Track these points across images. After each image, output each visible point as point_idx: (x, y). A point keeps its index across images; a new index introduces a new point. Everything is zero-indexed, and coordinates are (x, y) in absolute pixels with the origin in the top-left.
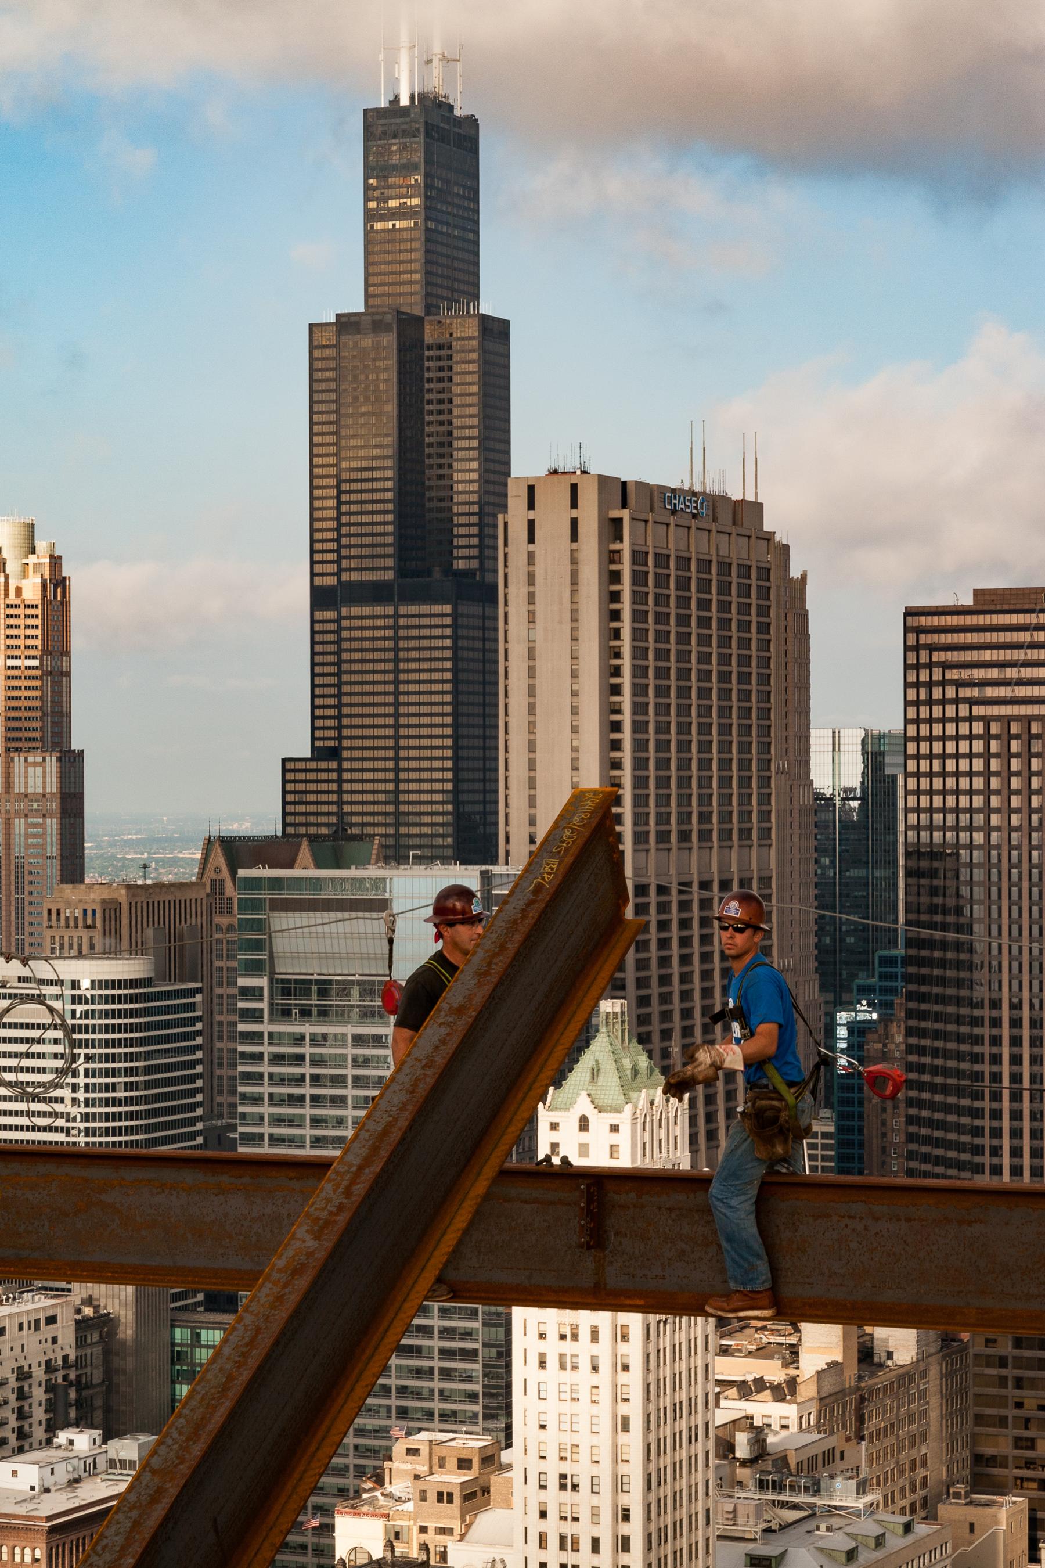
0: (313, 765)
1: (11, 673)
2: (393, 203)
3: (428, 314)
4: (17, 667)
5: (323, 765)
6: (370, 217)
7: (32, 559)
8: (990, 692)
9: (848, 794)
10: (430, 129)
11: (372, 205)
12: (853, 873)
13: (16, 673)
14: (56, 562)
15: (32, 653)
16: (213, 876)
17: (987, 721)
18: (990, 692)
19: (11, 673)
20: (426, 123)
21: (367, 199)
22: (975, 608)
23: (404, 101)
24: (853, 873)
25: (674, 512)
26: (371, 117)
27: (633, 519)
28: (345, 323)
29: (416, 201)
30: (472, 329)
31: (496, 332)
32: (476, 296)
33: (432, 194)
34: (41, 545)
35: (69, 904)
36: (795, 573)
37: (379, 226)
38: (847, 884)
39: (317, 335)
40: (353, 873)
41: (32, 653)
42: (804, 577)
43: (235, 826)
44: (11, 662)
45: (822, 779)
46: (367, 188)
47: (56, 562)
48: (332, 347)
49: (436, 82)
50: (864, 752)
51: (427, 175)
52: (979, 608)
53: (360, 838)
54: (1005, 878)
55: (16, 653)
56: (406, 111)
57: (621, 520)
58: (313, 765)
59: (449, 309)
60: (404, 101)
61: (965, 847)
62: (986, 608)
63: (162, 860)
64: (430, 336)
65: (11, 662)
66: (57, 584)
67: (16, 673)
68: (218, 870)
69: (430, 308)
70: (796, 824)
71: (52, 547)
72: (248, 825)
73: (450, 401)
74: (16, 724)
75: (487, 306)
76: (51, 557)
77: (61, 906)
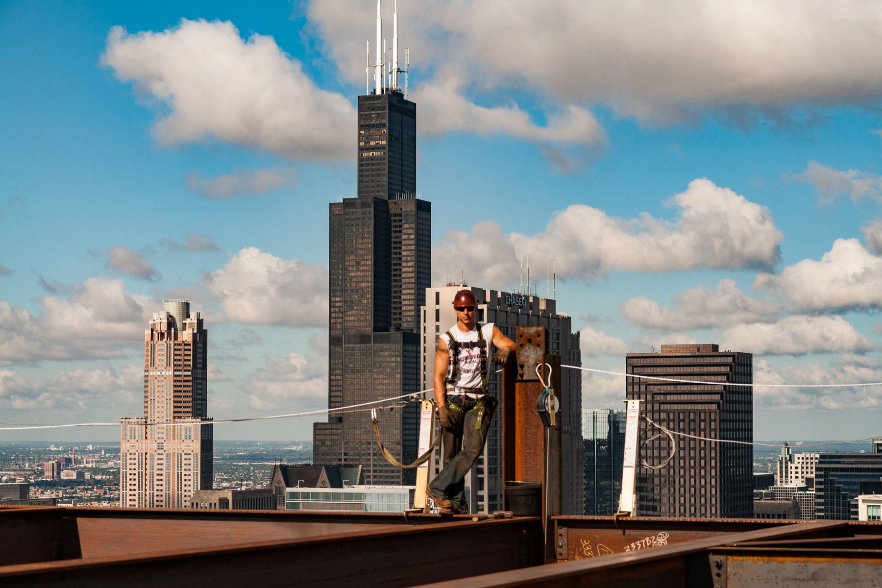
0: (329, 426)
1: (176, 378)
2: (372, 143)
3: (390, 198)
4: (180, 376)
5: (334, 426)
6: (361, 149)
7: (188, 321)
8: (670, 398)
9: (601, 442)
10: (391, 107)
11: (362, 144)
12: (603, 483)
13: (179, 378)
14: (200, 323)
15: (188, 368)
16: (277, 485)
17: (668, 412)
18: (670, 398)
19: (176, 378)
20: (389, 103)
21: (359, 141)
22: (661, 355)
23: (378, 92)
24: (603, 483)
25: (510, 306)
26: (360, 98)
27: (488, 309)
28: (348, 203)
29: (384, 142)
30: (412, 207)
31: (424, 207)
32: (414, 190)
33: (392, 139)
34: (193, 314)
35: (202, 501)
36: (574, 331)
37: (365, 154)
38: (601, 489)
39: (334, 209)
40: (346, 489)
41: (188, 368)
42: (578, 333)
43: (295, 448)
44: (176, 373)
45: (587, 434)
46: (359, 134)
47: (200, 323)
48: (341, 216)
49: (393, 85)
50: (609, 422)
51: (389, 130)
52: (664, 355)
53: (352, 466)
54: (677, 492)
55: (180, 368)
56: (379, 97)
57: (482, 310)
58: (329, 426)
59: (401, 196)
60: (378, 92)
61: (657, 476)
62: (667, 355)
63: (257, 466)
64: (393, 210)
65: (176, 373)
66: (201, 335)
67: (179, 378)
68: (279, 482)
69: (391, 196)
70: (574, 459)
71: (198, 314)
72: (301, 447)
73: (401, 243)
74: (179, 405)
75: (419, 196)
76: (198, 319)
77: (198, 501)
